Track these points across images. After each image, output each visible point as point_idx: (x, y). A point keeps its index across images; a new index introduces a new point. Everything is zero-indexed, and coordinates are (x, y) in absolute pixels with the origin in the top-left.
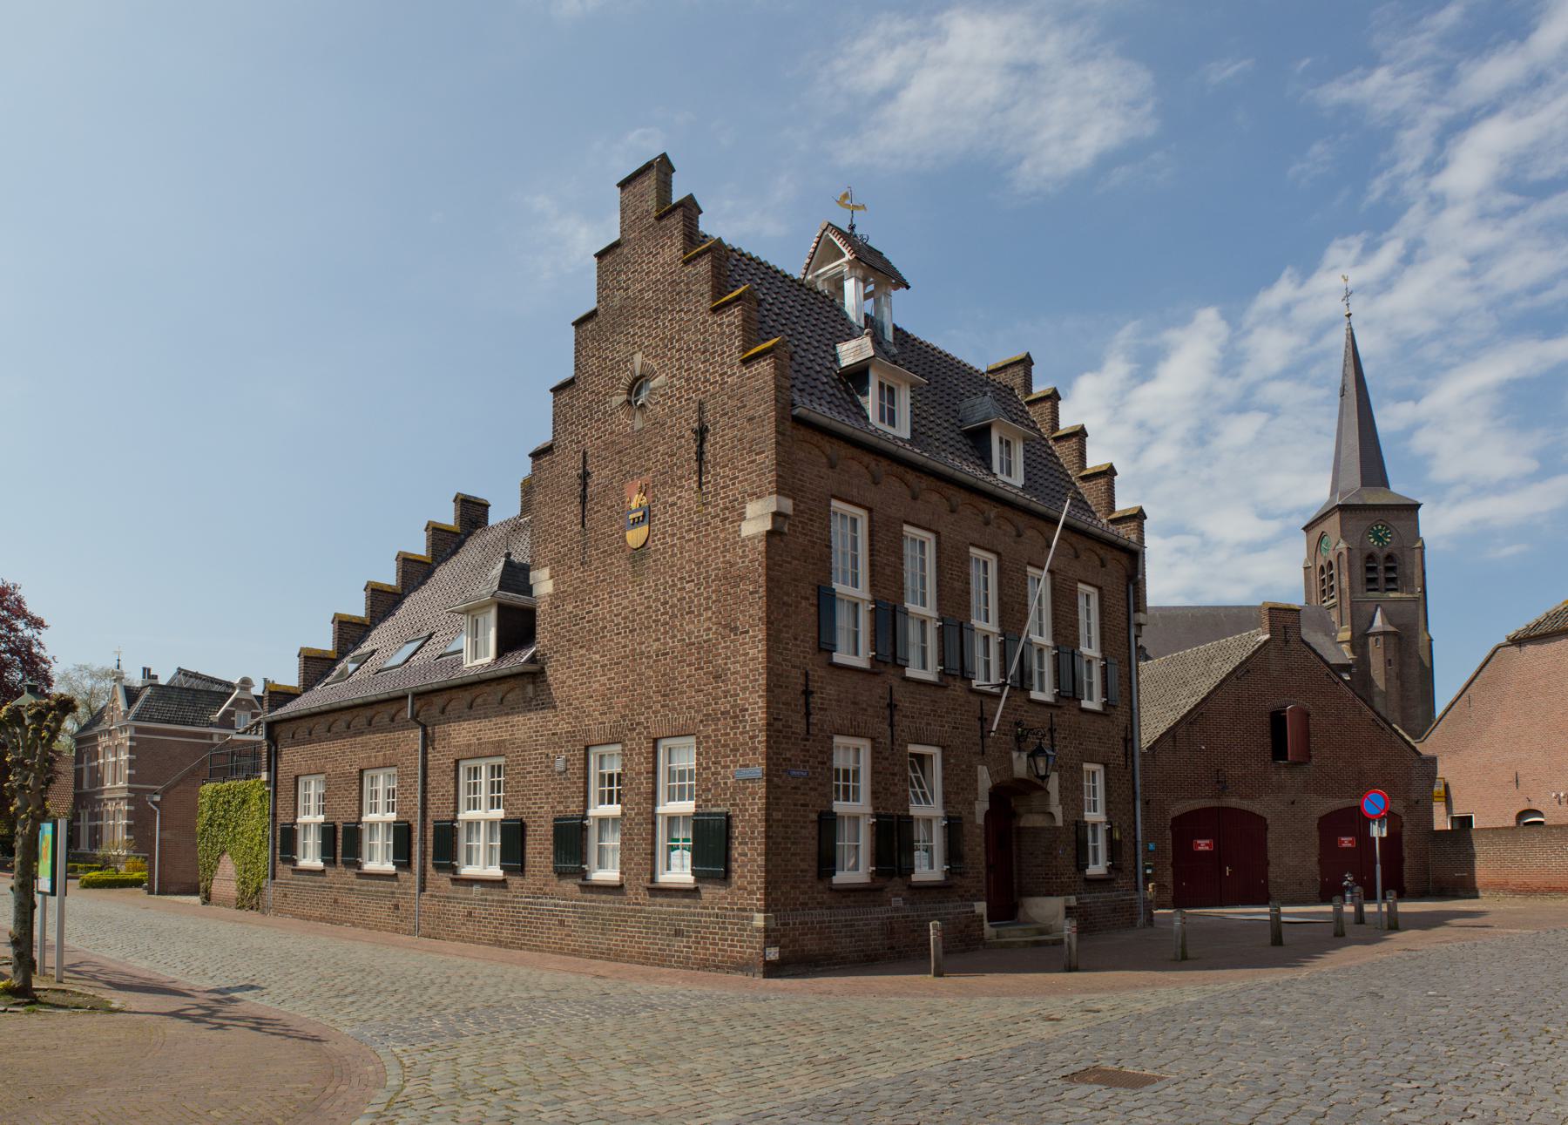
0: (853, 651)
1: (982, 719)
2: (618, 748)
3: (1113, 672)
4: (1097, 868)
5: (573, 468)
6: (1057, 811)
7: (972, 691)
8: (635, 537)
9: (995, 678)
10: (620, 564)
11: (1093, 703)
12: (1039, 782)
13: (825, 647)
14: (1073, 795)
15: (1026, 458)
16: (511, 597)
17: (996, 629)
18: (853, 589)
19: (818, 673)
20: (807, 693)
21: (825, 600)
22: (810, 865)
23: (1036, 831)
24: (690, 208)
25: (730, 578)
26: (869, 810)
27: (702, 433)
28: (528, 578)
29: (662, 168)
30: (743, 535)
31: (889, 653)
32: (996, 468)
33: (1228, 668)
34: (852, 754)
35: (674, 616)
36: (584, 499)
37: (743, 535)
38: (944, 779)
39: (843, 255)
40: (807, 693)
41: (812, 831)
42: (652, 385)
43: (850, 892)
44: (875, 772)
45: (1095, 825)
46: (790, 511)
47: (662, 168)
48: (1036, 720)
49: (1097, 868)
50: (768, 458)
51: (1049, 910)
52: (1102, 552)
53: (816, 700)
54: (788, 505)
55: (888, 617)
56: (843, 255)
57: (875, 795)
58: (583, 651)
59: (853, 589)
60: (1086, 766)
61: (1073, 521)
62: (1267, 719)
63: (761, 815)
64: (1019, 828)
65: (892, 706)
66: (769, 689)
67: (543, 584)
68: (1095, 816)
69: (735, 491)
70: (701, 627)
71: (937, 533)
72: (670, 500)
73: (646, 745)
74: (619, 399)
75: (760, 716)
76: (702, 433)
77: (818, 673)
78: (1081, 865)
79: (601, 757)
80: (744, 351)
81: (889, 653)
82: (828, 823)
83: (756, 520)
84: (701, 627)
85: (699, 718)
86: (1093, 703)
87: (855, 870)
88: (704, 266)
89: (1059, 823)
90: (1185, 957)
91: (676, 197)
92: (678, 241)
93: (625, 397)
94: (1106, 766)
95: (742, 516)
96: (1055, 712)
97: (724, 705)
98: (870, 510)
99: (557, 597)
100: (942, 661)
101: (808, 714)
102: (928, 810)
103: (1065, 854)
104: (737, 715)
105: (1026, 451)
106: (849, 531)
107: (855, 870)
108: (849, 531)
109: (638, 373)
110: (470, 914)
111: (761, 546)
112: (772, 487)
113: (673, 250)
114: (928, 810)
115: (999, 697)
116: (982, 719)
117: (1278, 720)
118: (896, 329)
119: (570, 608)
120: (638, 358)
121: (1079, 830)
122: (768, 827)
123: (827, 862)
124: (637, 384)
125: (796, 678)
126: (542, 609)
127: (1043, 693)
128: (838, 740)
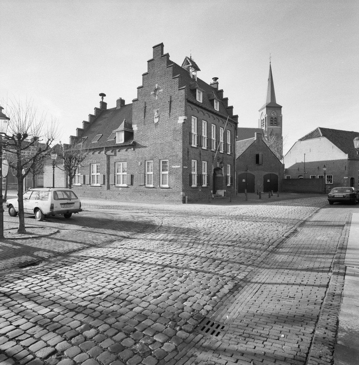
0: (195, 145)
1: (213, 156)
2: (152, 161)
3: (232, 147)
4: (229, 185)
5: (143, 105)
6: (223, 173)
7: (212, 151)
8: (156, 121)
9: (215, 148)
10: (153, 126)
11: (229, 153)
12: (221, 168)
13: (191, 143)
14: (226, 172)
15: (203, 96)
16: (128, 130)
17: (215, 139)
18: (194, 131)
19: (190, 148)
20: (188, 152)
21: (190, 134)
22: (188, 183)
23: (220, 177)
24: (168, 55)
25: (175, 130)
26: (196, 173)
27: (171, 102)
28: (132, 126)
29: (162, 45)
30: (178, 123)
31: (200, 144)
32: (215, 108)
33: (249, 145)
34: (194, 163)
35: (164, 137)
36: (145, 112)
37: (178, 123)
38: (207, 168)
39: (189, 64)
40: (188, 152)
41: (189, 177)
42: (160, 91)
43: (229, 187)
44: (197, 166)
45: (205, 175)
46: (186, 119)
47: (162, 45)
48: (221, 156)
49: (229, 185)
50: (183, 109)
51: (221, 193)
52: (231, 124)
53: (189, 153)
54: (186, 118)
55: (200, 138)
56: (189, 64)
57: (197, 170)
58: (144, 142)
59: (194, 131)
60: (203, 162)
61: (350, 185)
62: (255, 156)
63: (181, 174)
64: (217, 177)
65: (200, 154)
66: (183, 152)
67: (135, 128)
68: (229, 174)
69: (177, 114)
70: (169, 139)
71: (207, 122)
72: (164, 114)
73: (158, 161)
74: (152, 93)
75: (181, 156)
76: (171, 102)
77: (190, 148)
78: (226, 185)
79: (148, 163)
80: (179, 88)
81: (200, 144)
82: (191, 175)
83: (181, 120)
84: (169, 139)
85: (169, 156)
86: (229, 153)
87: (194, 185)
88: (171, 69)
89: (224, 176)
90: (231, 202)
91: (165, 53)
92: (166, 62)
93: (154, 92)
94: (231, 165)
95: (178, 119)
96: (224, 155)
97: (174, 154)
98: (197, 118)
99: (139, 131)
100: (207, 146)
101: (188, 156)
102: (205, 173)
103: (224, 181)
104: (177, 156)
105: (203, 94)
106: (194, 121)
107: (194, 185)
108: (194, 121)
109: (157, 88)
110: (119, 194)
111: (182, 125)
112: (184, 114)
113: (165, 64)
114: (205, 173)
115: (216, 152)
116: (213, 156)
117: (257, 156)
118: (197, 78)
119: (141, 133)
120: (157, 85)
121: (227, 177)
122: (183, 176)
123: (191, 183)
124: (156, 90)
125: (187, 149)
126: (135, 133)
127: (222, 152)
128: (192, 160)
